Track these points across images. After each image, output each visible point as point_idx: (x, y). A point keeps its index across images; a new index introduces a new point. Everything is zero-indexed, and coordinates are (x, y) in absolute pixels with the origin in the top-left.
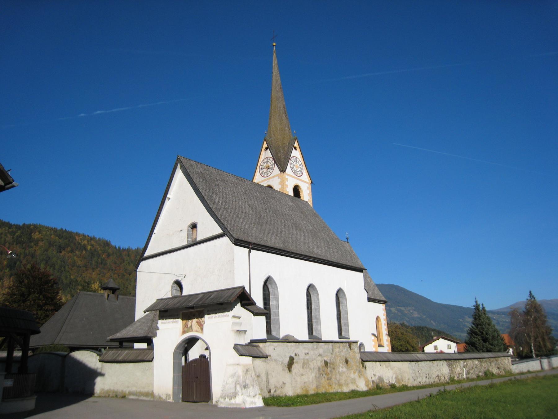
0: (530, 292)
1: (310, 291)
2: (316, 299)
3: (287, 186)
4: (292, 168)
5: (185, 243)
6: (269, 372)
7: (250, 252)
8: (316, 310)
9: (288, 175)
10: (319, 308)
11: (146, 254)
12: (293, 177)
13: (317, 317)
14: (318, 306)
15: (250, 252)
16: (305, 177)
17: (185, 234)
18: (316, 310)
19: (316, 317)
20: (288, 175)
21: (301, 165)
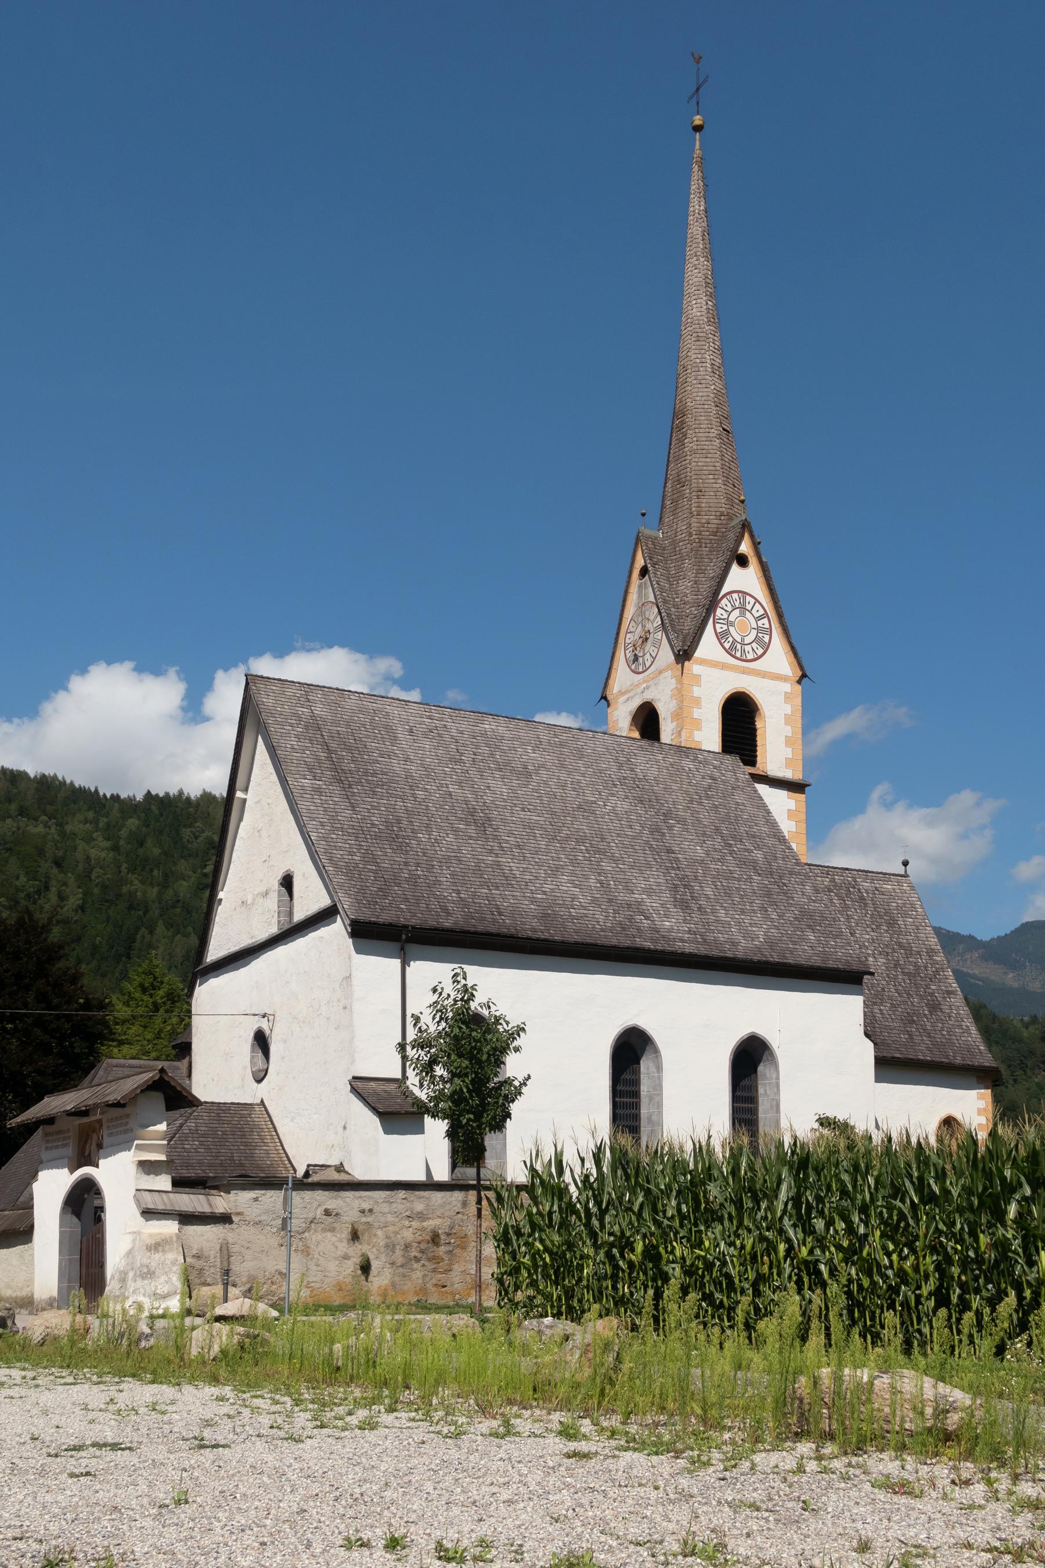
0: (529, 1077)
1: (631, 1050)
2: (653, 1069)
3: (697, 702)
4: (721, 637)
5: (274, 930)
6: (234, 1249)
7: (404, 965)
8: (651, 1098)
9: (703, 662)
10: (661, 1095)
11: (215, 952)
12: (724, 666)
13: (654, 1118)
14: (658, 1087)
15: (404, 965)
16: (778, 658)
17: (272, 903)
18: (651, 1098)
19: (649, 1119)
20: (703, 662)
21: (766, 615)
